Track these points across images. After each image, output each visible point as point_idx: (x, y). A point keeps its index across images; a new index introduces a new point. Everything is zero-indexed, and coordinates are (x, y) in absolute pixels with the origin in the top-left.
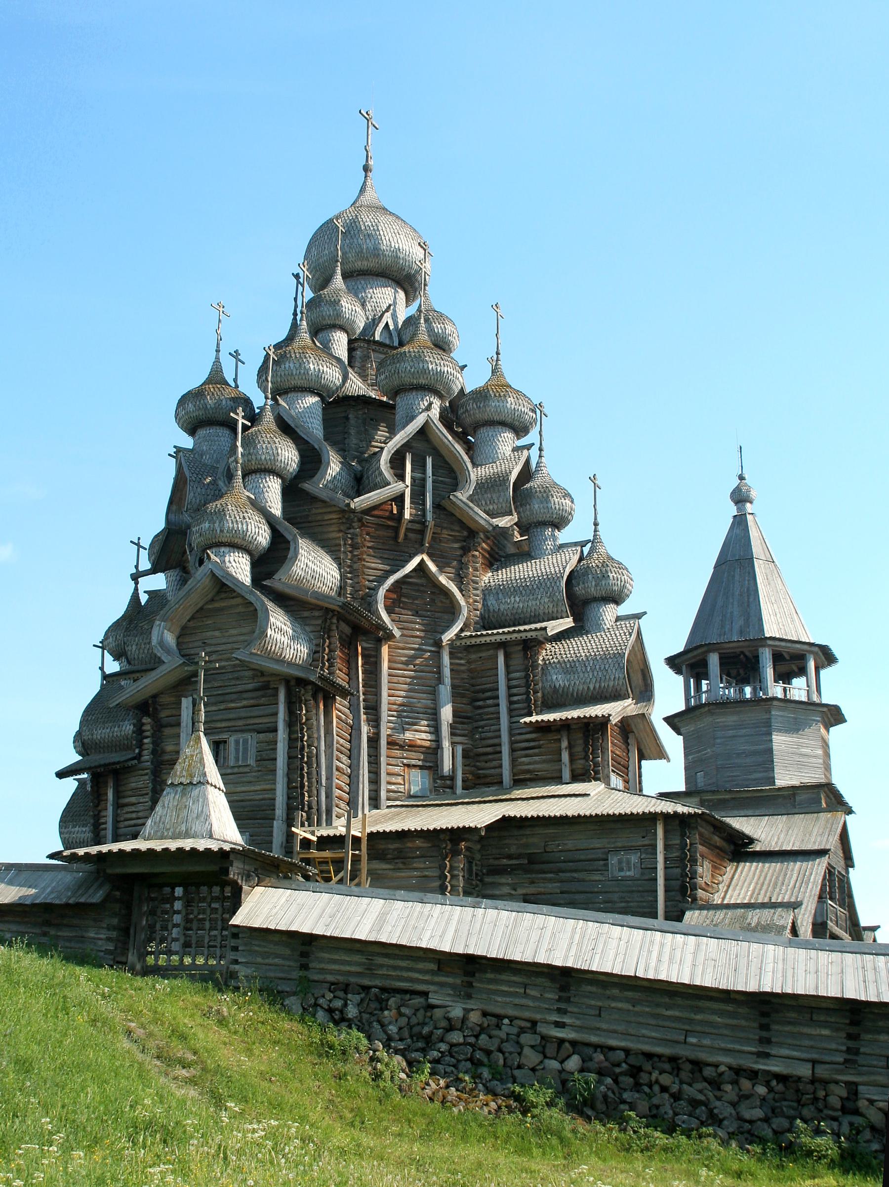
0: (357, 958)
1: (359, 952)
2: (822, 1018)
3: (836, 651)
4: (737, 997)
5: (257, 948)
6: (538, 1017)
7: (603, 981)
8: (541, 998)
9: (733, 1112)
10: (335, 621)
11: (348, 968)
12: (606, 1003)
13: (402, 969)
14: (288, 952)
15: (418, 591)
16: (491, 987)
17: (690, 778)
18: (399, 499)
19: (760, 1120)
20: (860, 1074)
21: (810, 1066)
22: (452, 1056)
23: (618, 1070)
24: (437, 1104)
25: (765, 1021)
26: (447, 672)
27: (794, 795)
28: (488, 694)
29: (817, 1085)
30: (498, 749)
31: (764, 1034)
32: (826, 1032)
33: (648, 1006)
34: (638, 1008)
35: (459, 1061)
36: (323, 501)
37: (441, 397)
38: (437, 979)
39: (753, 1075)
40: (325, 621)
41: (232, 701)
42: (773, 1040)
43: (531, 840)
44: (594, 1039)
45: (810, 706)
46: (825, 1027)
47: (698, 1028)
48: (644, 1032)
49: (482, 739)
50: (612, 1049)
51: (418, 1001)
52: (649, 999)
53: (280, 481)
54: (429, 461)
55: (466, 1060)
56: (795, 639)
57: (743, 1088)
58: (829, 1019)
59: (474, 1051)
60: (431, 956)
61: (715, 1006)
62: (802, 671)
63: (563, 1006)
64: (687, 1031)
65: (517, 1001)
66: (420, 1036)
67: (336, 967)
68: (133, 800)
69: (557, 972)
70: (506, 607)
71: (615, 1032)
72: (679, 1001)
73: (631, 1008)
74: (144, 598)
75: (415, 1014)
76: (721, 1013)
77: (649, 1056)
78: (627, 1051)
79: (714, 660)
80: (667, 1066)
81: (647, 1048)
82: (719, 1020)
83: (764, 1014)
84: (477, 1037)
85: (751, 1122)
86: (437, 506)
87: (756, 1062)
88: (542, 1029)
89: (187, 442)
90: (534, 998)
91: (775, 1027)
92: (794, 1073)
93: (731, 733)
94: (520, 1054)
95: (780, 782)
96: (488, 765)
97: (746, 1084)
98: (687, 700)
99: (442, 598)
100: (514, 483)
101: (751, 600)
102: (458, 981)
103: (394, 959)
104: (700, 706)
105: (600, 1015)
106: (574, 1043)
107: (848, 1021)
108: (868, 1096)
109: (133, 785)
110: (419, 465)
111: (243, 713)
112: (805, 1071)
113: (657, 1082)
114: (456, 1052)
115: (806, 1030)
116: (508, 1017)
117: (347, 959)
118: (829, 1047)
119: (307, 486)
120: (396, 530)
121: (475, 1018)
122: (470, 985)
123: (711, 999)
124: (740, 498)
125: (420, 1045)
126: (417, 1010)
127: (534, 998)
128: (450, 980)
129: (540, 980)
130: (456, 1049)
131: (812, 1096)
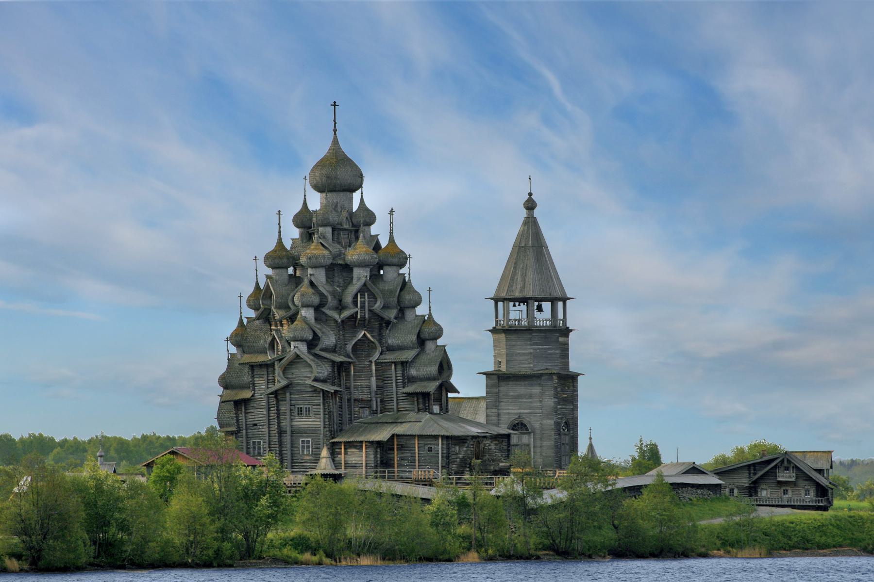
15: (363, 342)
18: (357, 313)
24: (163, 500)
26: (374, 371)
28: (389, 379)
30: (392, 399)
41: (304, 394)
43: (402, 440)
49: (387, 395)
54: (366, 294)
68: (252, 411)
74: (245, 321)
86: (370, 311)
96: (389, 404)
99: (372, 344)
101: (527, 272)
109: (252, 405)
111: (308, 398)
116: (429, 405)
120: (355, 321)
124: (530, 205)
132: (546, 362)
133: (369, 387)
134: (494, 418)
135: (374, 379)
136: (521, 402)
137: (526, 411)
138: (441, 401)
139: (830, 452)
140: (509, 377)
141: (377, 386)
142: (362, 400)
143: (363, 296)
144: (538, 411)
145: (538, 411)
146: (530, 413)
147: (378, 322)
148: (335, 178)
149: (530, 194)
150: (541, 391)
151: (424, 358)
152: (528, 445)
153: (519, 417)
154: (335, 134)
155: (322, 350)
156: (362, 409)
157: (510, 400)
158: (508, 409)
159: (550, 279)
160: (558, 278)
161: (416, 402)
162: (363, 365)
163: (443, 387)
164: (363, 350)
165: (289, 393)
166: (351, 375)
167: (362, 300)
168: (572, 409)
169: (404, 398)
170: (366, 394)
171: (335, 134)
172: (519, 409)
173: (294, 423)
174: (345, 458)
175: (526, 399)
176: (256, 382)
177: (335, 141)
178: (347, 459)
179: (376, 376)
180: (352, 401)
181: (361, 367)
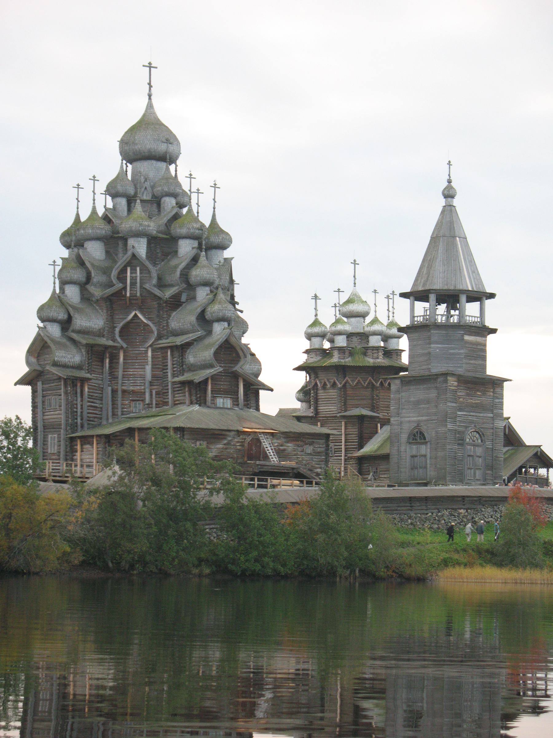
26: (150, 359)
54: (138, 269)
132: (447, 363)
133: (143, 377)
134: (396, 427)
135: (148, 368)
136: (420, 408)
137: (424, 418)
138: (238, 395)
139: (540, 446)
140: (411, 381)
141: (153, 376)
142: (133, 392)
143: (133, 271)
144: (434, 418)
145: (434, 418)
146: (427, 420)
147: (156, 301)
148: (133, 143)
149: (449, 181)
150: (437, 395)
151: (207, 341)
152: (425, 456)
153: (418, 426)
154: (150, 98)
155: (73, 331)
156: (134, 403)
157: (411, 407)
158: (409, 417)
159: (458, 271)
160: (473, 272)
161: (187, 394)
162: (137, 352)
163: (240, 378)
164: (137, 334)
165: (41, 382)
166: (118, 363)
167: (134, 275)
168: (492, 418)
169: (179, 389)
170: (139, 384)
171: (150, 98)
172: (418, 416)
173: (46, 417)
174: (81, 455)
175: (425, 404)
176: (319, 405)
177: (150, 106)
178: (83, 457)
179: (152, 365)
180: (120, 393)
181: (135, 354)
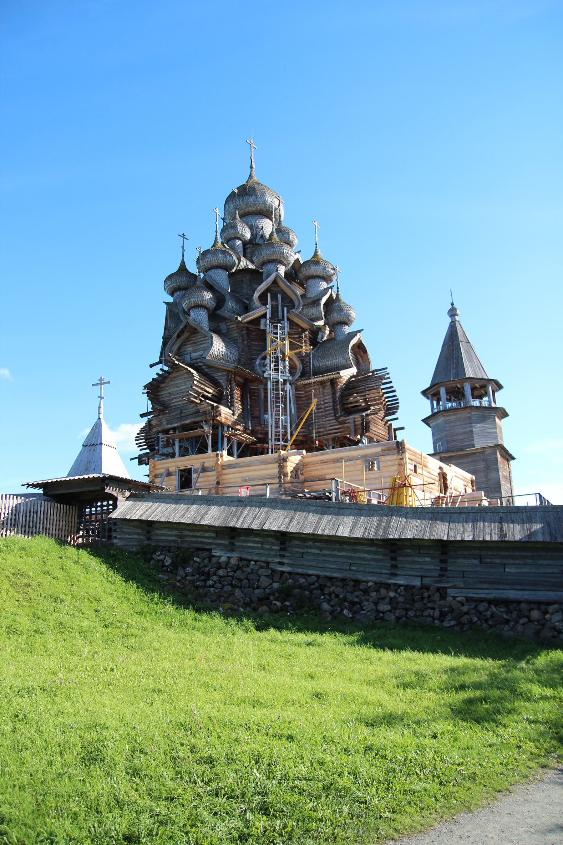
0: (175, 532)
1: (176, 529)
2: (426, 552)
3: (501, 382)
4: (378, 542)
5: (125, 530)
6: (270, 560)
7: (304, 538)
8: (272, 549)
9: (374, 607)
10: (233, 376)
11: (170, 538)
12: (306, 550)
13: (198, 537)
14: (140, 531)
16: (244, 544)
17: (435, 448)
19: (388, 611)
20: (448, 582)
21: (419, 579)
22: (220, 583)
23: (312, 587)
25: (393, 555)
27: (484, 452)
29: (423, 590)
31: (394, 563)
32: (428, 559)
33: (328, 550)
34: (324, 552)
35: (224, 586)
36: (228, 319)
37: (285, 265)
38: (216, 541)
39: (388, 586)
40: (228, 376)
42: (399, 565)
44: (300, 571)
45: (490, 408)
46: (428, 557)
47: (357, 562)
48: (327, 565)
50: (310, 575)
51: (206, 553)
52: (329, 546)
53: (206, 311)
54: (279, 296)
55: (228, 585)
56: (481, 377)
57: (382, 594)
58: (429, 552)
59: (233, 579)
60: (212, 529)
61: (366, 548)
62: (486, 394)
63: (282, 553)
64: (351, 563)
65: (257, 551)
66: (203, 573)
67: (165, 538)
69: (279, 534)
70: (323, 364)
71: (311, 566)
72: (345, 547)
73: (319, 552)
75: (203, 561)
76: (369, 552)
77: (330, 579)
78: (318, 576)
79: (443, 391)
80: (340, 584)
81: (328, 574)
82: (368, 556)
83: (393, 551)
84: (235, 572)
85: (383, 612)
87: (389, 579)
88: (272, 566)
89: (170, 300)
90: (267, 549)
91: (399, 558)
92: (411, 584)
93: (453, 424)
94: (258, 580)
95: (477, 446)
97: (383, 591)
98: (432, 411)
100: (324, 304)
102: (227, 542)
103: (194, 532)
104: (439, 412)
105: (303, 557)
106: (290, 573)
107: (440, 553)
108: (452, 594)
110: (274, 298)
112: (417, 583)
113: (333, 592)
114: (223, 581)
115: (417, 559)
117: (170, 533)
118: (430, 568)
119: (219, 312)
121: (233, 561)
122: (233, 544)
123: (363, 544)
124: (452, 312)
125: (203, 578)
126: (204, 559)
127: (267, 549)
128: (223, 542)
129: (269, 539)
130: (222, 579)
131: (420, 596)
